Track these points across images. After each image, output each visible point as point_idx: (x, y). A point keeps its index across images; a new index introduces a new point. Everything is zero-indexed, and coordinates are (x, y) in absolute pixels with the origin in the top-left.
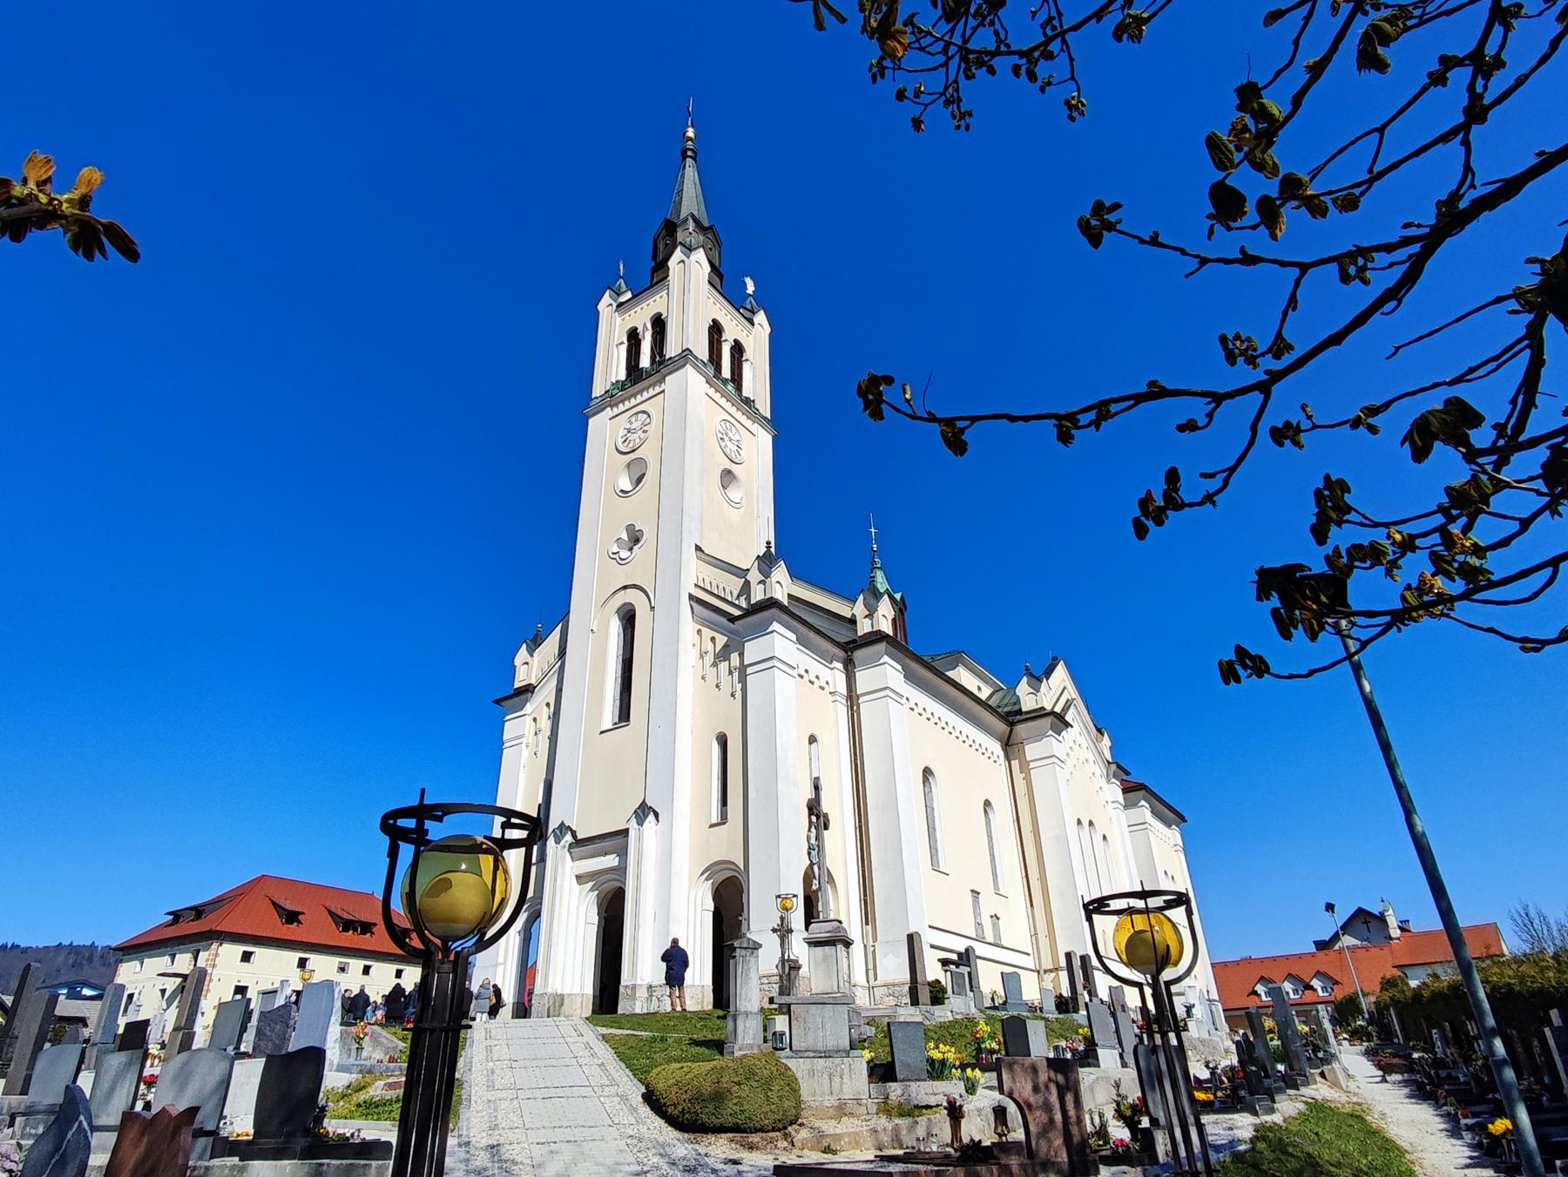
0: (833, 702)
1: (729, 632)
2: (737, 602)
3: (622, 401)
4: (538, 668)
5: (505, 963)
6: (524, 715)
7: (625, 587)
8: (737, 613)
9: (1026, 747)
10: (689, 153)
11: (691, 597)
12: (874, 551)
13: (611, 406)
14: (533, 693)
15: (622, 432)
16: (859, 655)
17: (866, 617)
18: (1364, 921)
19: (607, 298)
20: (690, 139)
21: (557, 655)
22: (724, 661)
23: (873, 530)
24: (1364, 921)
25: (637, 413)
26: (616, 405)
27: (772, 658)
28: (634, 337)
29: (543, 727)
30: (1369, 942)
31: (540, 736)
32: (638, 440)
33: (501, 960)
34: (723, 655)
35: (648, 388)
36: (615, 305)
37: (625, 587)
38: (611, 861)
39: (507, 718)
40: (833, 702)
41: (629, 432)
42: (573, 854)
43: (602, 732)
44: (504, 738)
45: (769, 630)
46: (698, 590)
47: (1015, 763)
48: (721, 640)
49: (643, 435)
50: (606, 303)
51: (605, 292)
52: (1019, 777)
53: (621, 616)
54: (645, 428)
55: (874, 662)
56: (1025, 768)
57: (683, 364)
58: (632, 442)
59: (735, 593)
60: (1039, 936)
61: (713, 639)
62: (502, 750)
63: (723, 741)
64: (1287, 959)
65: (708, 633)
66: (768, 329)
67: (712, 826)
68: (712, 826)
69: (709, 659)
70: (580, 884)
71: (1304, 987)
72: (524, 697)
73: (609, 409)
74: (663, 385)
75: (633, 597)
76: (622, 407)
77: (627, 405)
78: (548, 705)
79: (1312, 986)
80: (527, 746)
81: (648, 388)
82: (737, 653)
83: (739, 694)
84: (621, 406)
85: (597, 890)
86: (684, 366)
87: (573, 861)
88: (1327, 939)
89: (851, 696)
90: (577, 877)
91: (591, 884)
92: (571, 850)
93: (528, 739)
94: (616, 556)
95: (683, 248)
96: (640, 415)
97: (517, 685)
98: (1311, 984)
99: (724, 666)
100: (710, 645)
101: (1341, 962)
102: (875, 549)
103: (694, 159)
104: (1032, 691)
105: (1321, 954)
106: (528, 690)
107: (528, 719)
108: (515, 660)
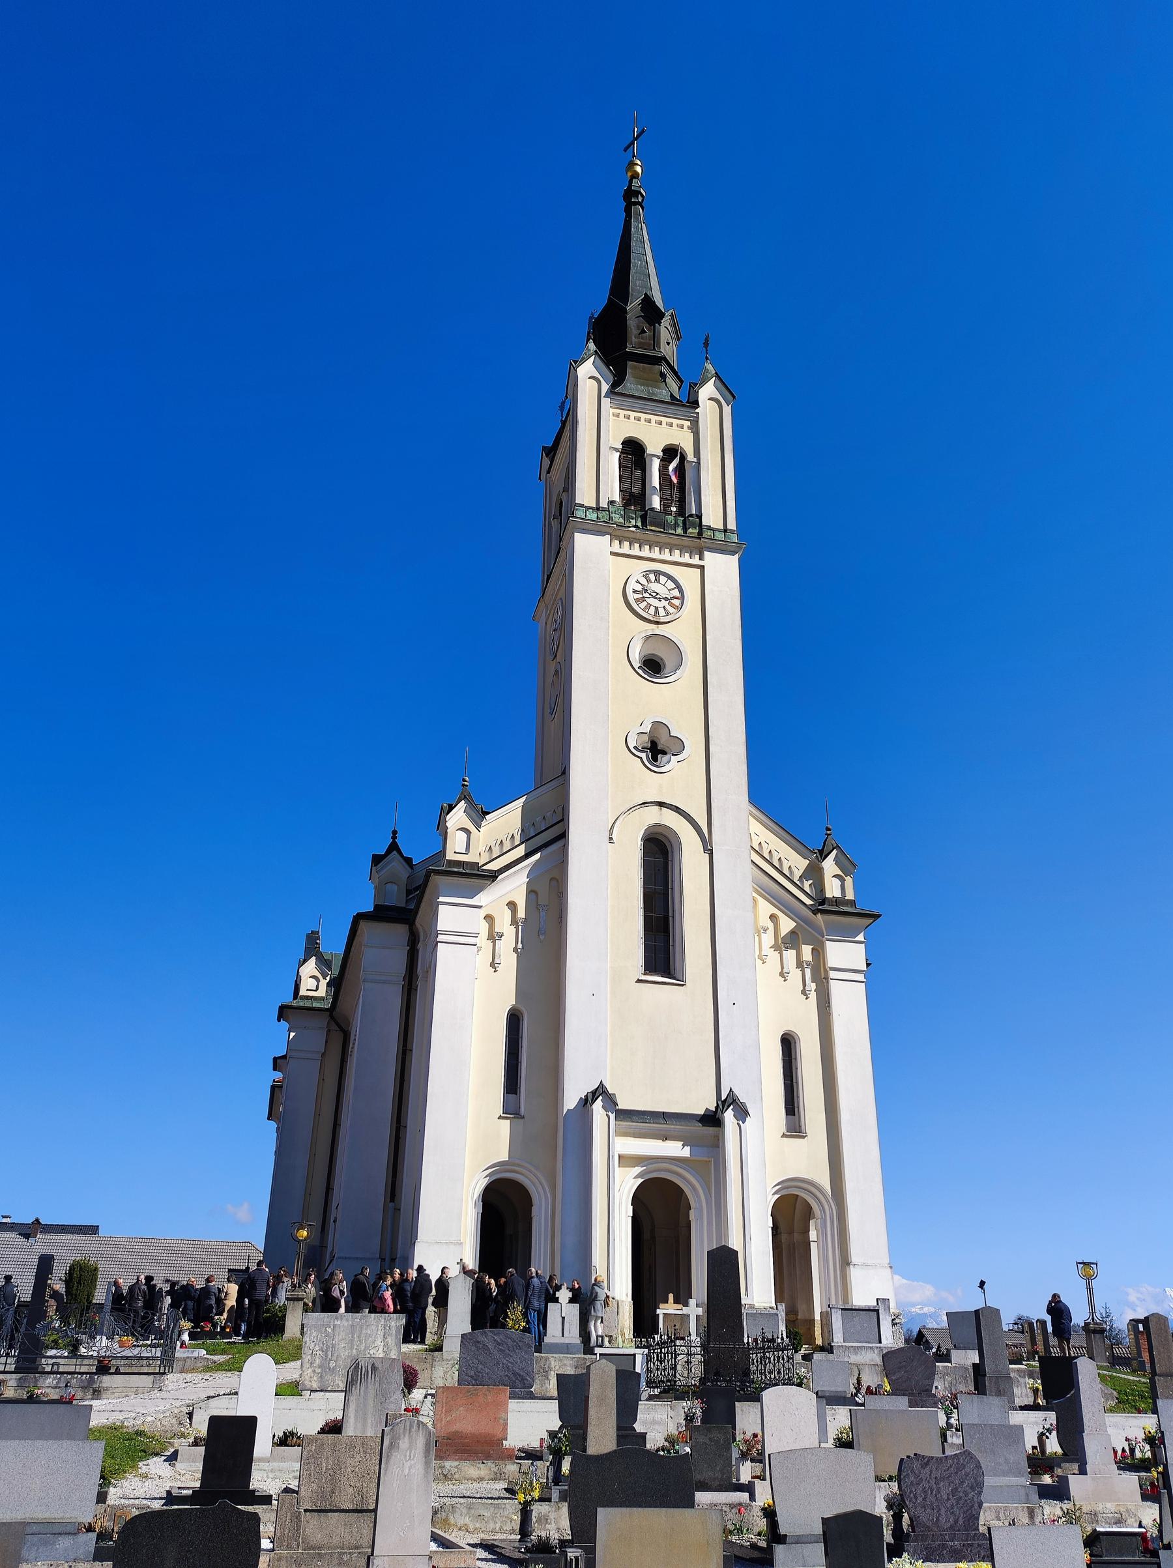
7: (661, 804)
21: (517, 841)
25: (658, 574)
37: (661, 804)
38: (675, 1149)
39: (441, 899)
48: (787, 925)
57: (732, 549)
73: (608, 537)
75: (670, 820)
77: (656, 554)
96: (663, 579)
99: (790, 955)
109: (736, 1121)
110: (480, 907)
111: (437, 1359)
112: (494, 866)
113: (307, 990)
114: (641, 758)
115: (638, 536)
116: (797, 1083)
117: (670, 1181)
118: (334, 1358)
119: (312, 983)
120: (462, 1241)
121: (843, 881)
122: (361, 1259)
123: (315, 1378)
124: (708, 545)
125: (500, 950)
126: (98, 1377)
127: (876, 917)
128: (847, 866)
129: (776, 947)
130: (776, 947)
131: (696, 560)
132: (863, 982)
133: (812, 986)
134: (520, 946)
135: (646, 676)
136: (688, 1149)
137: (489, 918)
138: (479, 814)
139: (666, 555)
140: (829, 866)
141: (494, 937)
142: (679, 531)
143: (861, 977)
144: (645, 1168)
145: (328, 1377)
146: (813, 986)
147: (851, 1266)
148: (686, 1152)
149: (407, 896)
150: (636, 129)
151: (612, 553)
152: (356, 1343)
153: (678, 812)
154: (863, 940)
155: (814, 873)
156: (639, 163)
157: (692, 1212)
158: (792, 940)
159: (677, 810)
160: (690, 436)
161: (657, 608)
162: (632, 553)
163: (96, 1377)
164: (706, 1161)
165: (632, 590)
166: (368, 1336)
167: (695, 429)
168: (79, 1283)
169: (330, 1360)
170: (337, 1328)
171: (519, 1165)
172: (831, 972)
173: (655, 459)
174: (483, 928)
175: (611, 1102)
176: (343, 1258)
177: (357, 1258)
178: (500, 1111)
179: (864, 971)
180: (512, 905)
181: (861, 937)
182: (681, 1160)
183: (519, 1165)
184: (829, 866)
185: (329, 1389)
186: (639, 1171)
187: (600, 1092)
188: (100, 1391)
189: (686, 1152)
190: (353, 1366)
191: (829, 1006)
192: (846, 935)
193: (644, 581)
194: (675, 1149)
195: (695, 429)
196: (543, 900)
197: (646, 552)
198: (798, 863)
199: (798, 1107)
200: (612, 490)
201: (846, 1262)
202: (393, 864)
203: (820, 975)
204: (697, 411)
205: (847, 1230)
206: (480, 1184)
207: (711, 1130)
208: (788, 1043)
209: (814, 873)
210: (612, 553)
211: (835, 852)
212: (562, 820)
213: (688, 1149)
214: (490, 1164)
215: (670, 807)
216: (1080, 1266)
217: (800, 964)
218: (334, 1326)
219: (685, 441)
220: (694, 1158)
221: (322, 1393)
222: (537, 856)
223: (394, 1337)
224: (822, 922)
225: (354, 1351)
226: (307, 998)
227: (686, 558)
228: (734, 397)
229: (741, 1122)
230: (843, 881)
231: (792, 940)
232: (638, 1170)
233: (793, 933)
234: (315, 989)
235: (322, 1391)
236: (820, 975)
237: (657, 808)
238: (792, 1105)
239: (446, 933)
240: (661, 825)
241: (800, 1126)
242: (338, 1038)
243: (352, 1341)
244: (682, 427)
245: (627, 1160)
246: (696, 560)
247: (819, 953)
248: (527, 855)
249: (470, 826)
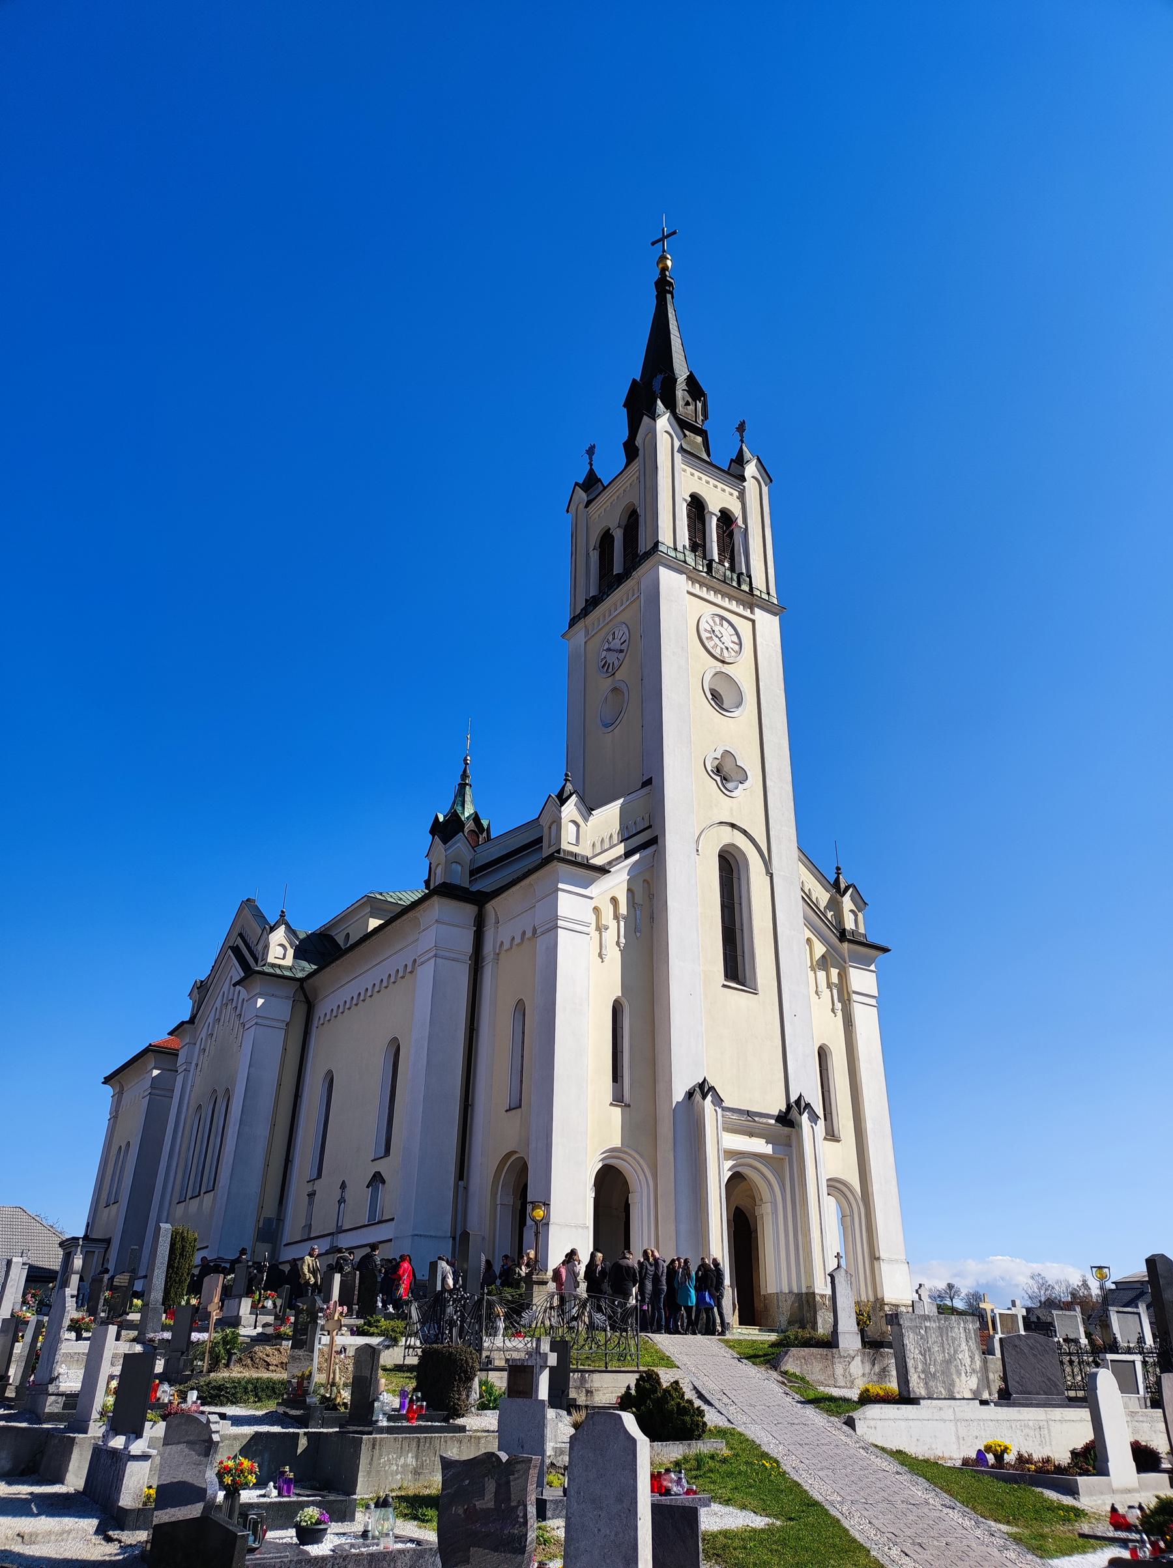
7: (733, 826)
21: (615, 840)
22: (822, 970)
25: (723, 618)
37: (733, 826)
38: (760, 1146)
39: (560, 886)
48: (820, 949)
57: (776, 611)
77: (726, 603)
83: (839, 1013)
99: (822, 975)
109: (809, 1123)
110: (592, 898)
111: (836, 1356)
112: (598, 861)
113: (275, 958)
115: (706, 582)
116: (829, 1091)
117: (729, 1178)
118: (932, 1363)
119: (280, 951)
120: (587, 1225)
121: (856, 916)
122: (435, 1237)
123: (922, 1385)
125: (606, 942)
126: (589, 1375)
127: (885, 950)
128: (861, 903)
131: (747, 613)
132: (875, 1006)
133: (838, 1006)
134: (623, 940)
135: (717, 708)
137: (596, 910)
138: (588, 807)
140: (847, 902)
141: (600, 928)
142: (735, 584)
143: (873, 1002)
144: (735, 1162)
145: (931, 1383)
147: (881, 1261)
148: (768, 1149)
149: (470, 877)
150: (665, 229)
151: (689, 593)
152: (946, 1347)
154: (874, 969)
155: (834, 905)
156: (669, 257)
158: (823, 963)
159: (745, 832)
160: (739, 505)
163: (587, 1375)
164: (780, 1159)
165: (703, 629)
166: (954, 1339)
167: (742, 497)
168: (182, 1255)
169: (930, 1365)
170: (928, 1330)
172: (854, 995)
173: (714, 517)
174: (592, 919)
175: (718, 1101)
176: (417, 1235)
177: (431, 1236)
178: (610, 1099)
179: (876, 997)
180: (614, 900)
181: (872, 967)
182: (762, 1156)
184: (847, 902)
185: (935, 1396)
186: (731, 1165)
187: (704, 1089)
188: (592, 1392)
189: (768, 1149)
191: (852, 1025)
192: (865, 962)
194: (760, 1146)
195: (742, 497)
196: (639, 899)
198: (822, 896)
199: (831, 1114)
200: (684, 538)
201: (875, 1258)
202: (458, 844)
203: (844, 996)
204: (744, 484)
205: (874, 1227)
207: (787, 1130)
208: (823, 1054)
210: (689, 593)
211: (851, 890)
212: (650, 827)
214: (604, 1150)
215: (740, 829)
216: (1094, 1270)
217: (829, 986)
218: (926, 1327)
219: (736, 509)
220: (776, 1156)
221: (929, 1401)
222: (636, 857)
223: (974, 1341)
224: (846, 951)
225: (946, 1355)
226: (273, 966)
227: (740, 610)
228: (771, 481)
229: (813, 1125)
230: (856, 916)
231: (823, 963)
234: (282, 957)
235: (929, 1398)
236: (844, 996)
237: (729, 829)
239: (566, 919)
240: (733, 845)
241: (833, 1131)
242: (302, 1009)
243: (943, 1343)
244: (731, 494)
247: (843, 976)
248: (628, 855)
249: (580, 820)
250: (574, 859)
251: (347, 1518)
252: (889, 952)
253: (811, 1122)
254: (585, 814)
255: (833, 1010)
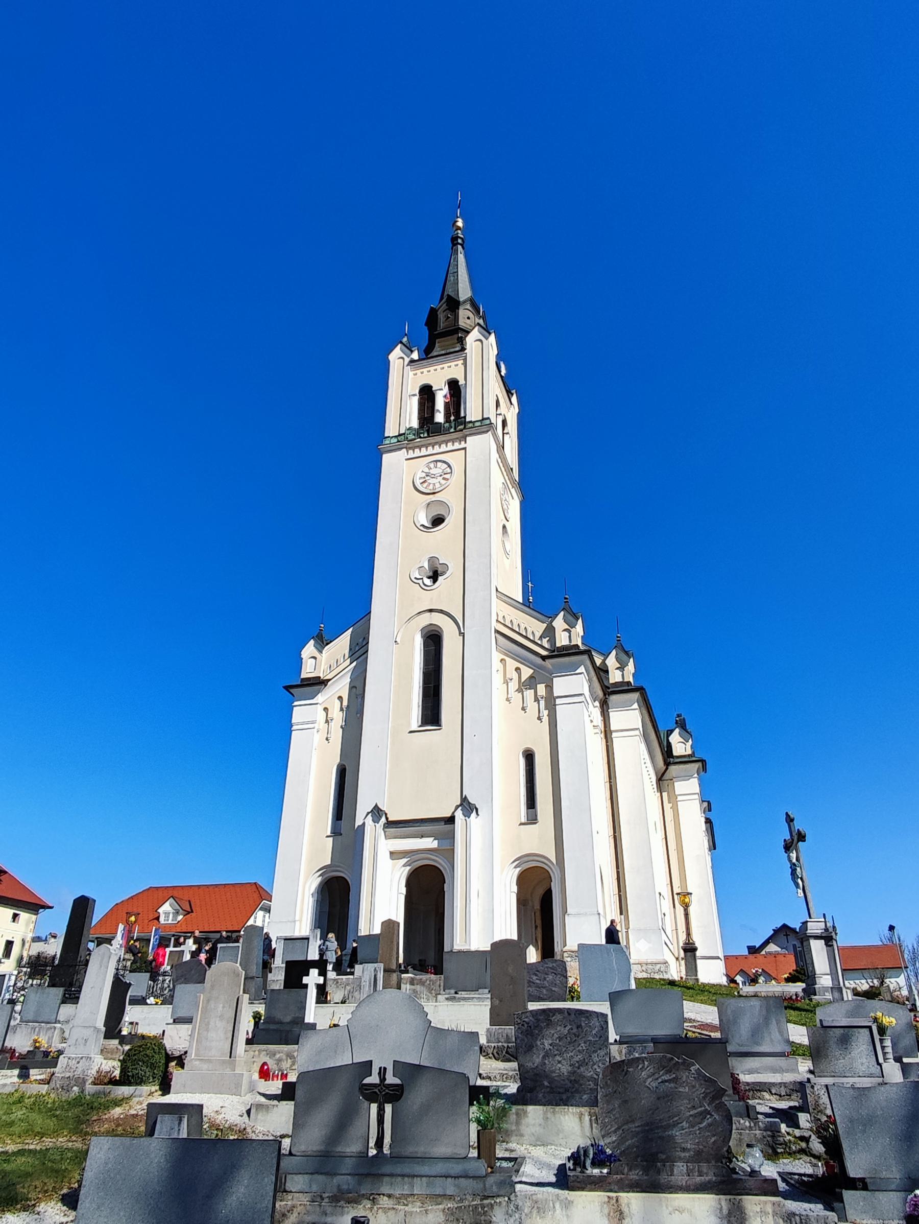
0: (595, 734)
1: (535, 666)
2: (539, 642)
3: (420, 447)
4: (325, 665)
5: (301, 921)
6: (317, 704)
7: (431, 611)
8: (544, 653)
9: (676, 784)
10: (460, 241)
11: (497, 632)
12: (531, 602)
13: (408, 449)
14: (326, 685)
15: (420, 474)
16: (614, 698)
17: (617, 669)
18: (785, 934)
19: (397, 352)
20: (459, 228)
21: (347, 656)
22: (529, 689)
23: (530, 585)
24: (785, 934)
25: (436, 461)
26: (413, 449)
27: (581, 695)
28: (427, 393)
29: (335, 716)
30: (787, 950)
31: (332, 724)
32: (437, 485)
33: (297, 918)
34: (531, 683)
35: (446, 442)
36: (407, 360)
37: (431, 611)
38: (429, 843)
39: (296, 703)
40: (595, 734)
41: (427, 476)
42: (386, 833)
43: (411, 732)
44: (293, 721)
45: (577, 672)
46: (499, 625)
47: (665, 794)
48: (527, 672)
49: (443, 482)
50: (396, 356)
51: (397, 345)
52: (667, 806)
53: (423, 634)
54: (446, 476)
55: (626, 706)
56: (673, 799)
57: (486, 430)
58: (431, 485)
59: (538, 635)
60: (679, 930)
61: (517, 669)
62: (291, 731)
63: (529, 757)
64: (737, 958)
65: (512, 664)
66: (517, 410)
67: (521, 824)
68: (521, 824)
69: (514, 685)
70: (392, 860)
71: (730, 981)
72: (316, 688)
73: (405, 450)
74: (463, 443)
75: (438, 620)
76: (417, 453)
77: (430, 450)
78: (340, 698)
79: (736, 981)
80: (318, 732)
81: (442, 442)
82: (544, 685)
83: (545, 719)
84: (417, 450)
85: (409, 865)
86: (488, 431)
87: (386, 839)
88: (757, 946)
89: (605, 731)
90: (391, 853)
91: (405, 860)
92: (386, 830)
93: (319, 726)
94: (420, 582)
95: (481, 329)
96: (439, 464)
97: (304, 675)
98: (735, 979)
99: (529, 694)
100: (515, 676)
101: (776, 963)
102: (531, 600)
103: (462, 245)
104: (683, 740)
105: (751, 957)
106: (319, 683)
107: (320, 708)
108: (302, 653)
114: (419, 584)
124: (468, 433)
129: (520, 690)
130: (520, 690)
136: (436, 842)
138: (322, 642)
139: (437, 449)
144: (409, 859)
146: (546, 712)
153: (443, 613)
157: (445, 885)
159: (441, 611)
161: (434, 484)
162: (422, 454)
171: (339, 867)
183: (339, 867)
190: (703, 1036)
192: (571, 670)
193: (427, 470)
194: (429, 843)
197: (424, 452)
206: (314, 882)
209: (550, 632)
213: (436, 842)
217: (537, 700)
231: (531, 683)
232: (405, 860)
233: (531, 677)
237: (428, 614)
238: (531, 802)
245: (394, 855)
246: (463, 445)
247: (550, 687)
249: (317, 654)
250: (577, 651)
251: (162, 1086)
252: (284, 685)
253: (465, 817)
254: (320, 649)
255: (539, 718)
